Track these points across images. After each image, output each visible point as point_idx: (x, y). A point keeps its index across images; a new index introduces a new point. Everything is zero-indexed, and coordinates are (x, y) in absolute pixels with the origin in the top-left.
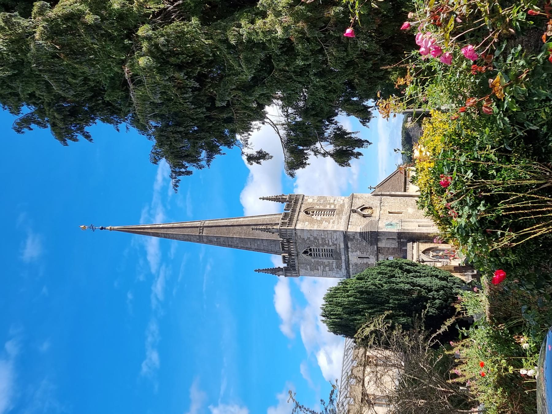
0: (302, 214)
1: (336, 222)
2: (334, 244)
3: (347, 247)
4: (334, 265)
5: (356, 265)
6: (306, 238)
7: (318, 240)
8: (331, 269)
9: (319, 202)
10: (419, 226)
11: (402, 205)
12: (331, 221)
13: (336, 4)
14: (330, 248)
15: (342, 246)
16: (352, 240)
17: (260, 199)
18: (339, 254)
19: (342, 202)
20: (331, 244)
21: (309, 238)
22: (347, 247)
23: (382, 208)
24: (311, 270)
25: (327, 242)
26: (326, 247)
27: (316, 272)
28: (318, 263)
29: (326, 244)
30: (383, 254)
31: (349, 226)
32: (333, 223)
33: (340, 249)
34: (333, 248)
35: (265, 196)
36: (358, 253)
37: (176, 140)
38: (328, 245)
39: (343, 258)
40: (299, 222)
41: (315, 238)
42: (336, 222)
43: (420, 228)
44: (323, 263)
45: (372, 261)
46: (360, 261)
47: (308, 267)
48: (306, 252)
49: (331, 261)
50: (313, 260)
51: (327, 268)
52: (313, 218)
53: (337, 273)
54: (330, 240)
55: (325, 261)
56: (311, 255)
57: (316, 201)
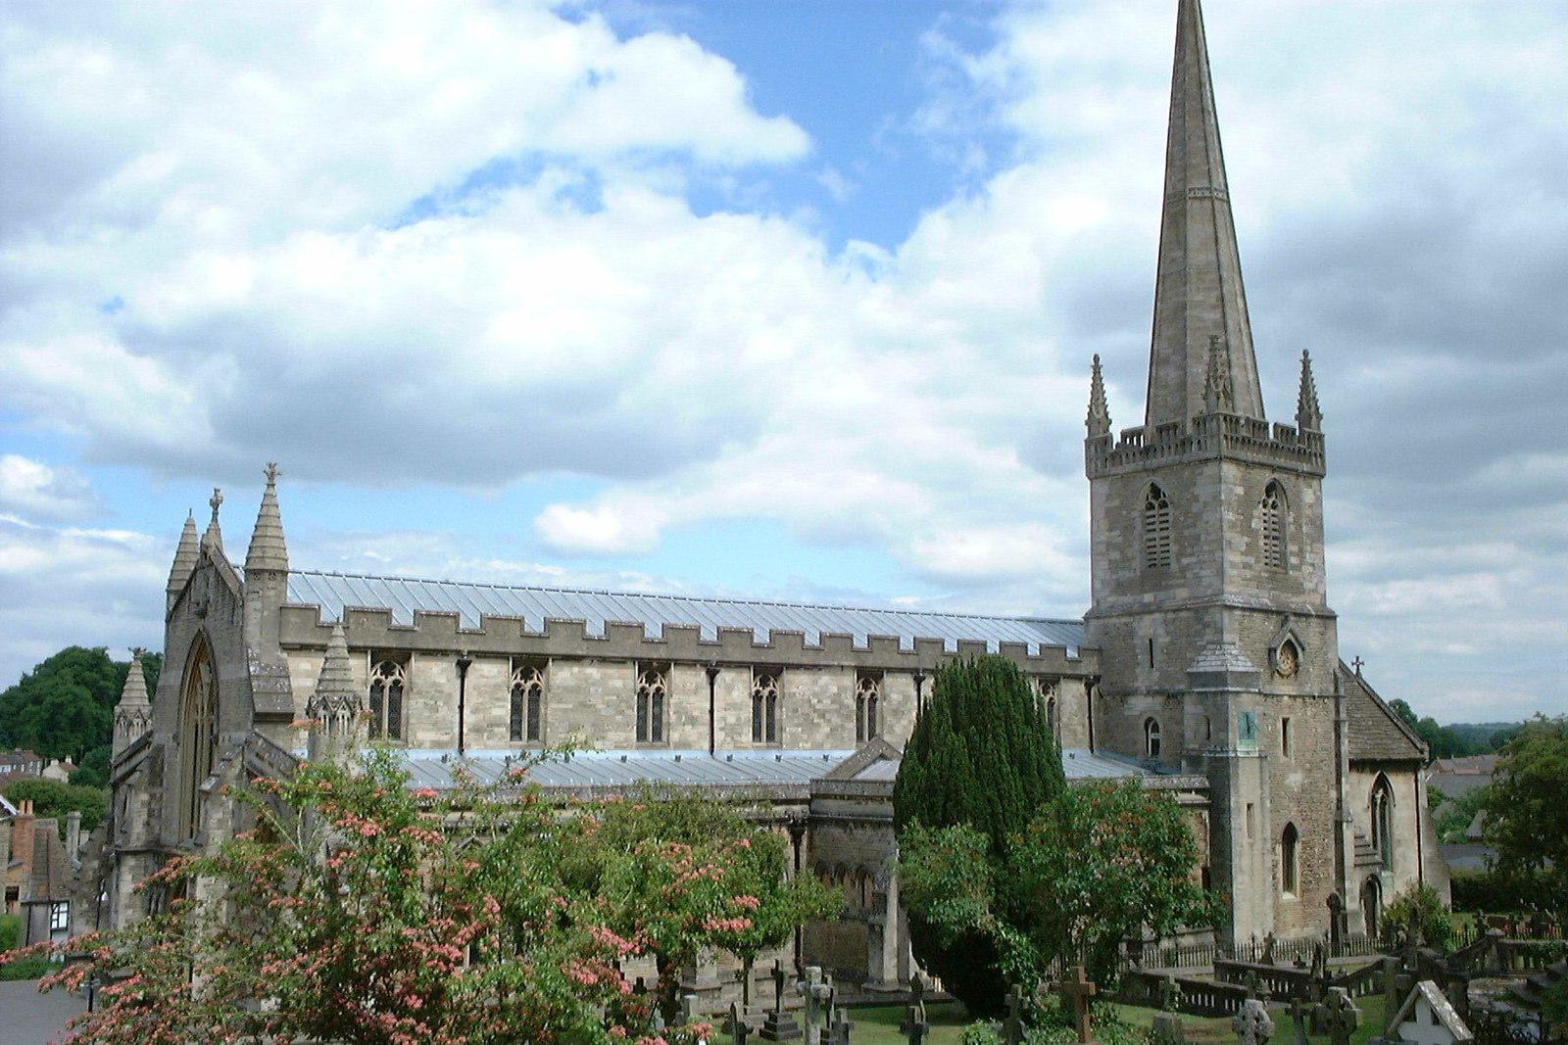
0: (1267, 477)
2: (1183, 570)
5: (1131, 633)
6: (1197, 491)
8: (1114, 566)
10: (1249, 806)
12: (1251, 560)
14: (1172, 561)
20: (1185, 561)
21: (1196, 499)
24: (1108, 511)
26: (1174, 548)
32: (1246, 566)
34: (1174, 567)
35: (1312, 367)
38: (1180, 555)
42: (1248, 574)
46: (1139, 642)
47: (1116, 503)
48: (1156, 491)
50: (1135, 514)
51: (1115, 555)
55: (1137, 546)
56: (1150, 507)
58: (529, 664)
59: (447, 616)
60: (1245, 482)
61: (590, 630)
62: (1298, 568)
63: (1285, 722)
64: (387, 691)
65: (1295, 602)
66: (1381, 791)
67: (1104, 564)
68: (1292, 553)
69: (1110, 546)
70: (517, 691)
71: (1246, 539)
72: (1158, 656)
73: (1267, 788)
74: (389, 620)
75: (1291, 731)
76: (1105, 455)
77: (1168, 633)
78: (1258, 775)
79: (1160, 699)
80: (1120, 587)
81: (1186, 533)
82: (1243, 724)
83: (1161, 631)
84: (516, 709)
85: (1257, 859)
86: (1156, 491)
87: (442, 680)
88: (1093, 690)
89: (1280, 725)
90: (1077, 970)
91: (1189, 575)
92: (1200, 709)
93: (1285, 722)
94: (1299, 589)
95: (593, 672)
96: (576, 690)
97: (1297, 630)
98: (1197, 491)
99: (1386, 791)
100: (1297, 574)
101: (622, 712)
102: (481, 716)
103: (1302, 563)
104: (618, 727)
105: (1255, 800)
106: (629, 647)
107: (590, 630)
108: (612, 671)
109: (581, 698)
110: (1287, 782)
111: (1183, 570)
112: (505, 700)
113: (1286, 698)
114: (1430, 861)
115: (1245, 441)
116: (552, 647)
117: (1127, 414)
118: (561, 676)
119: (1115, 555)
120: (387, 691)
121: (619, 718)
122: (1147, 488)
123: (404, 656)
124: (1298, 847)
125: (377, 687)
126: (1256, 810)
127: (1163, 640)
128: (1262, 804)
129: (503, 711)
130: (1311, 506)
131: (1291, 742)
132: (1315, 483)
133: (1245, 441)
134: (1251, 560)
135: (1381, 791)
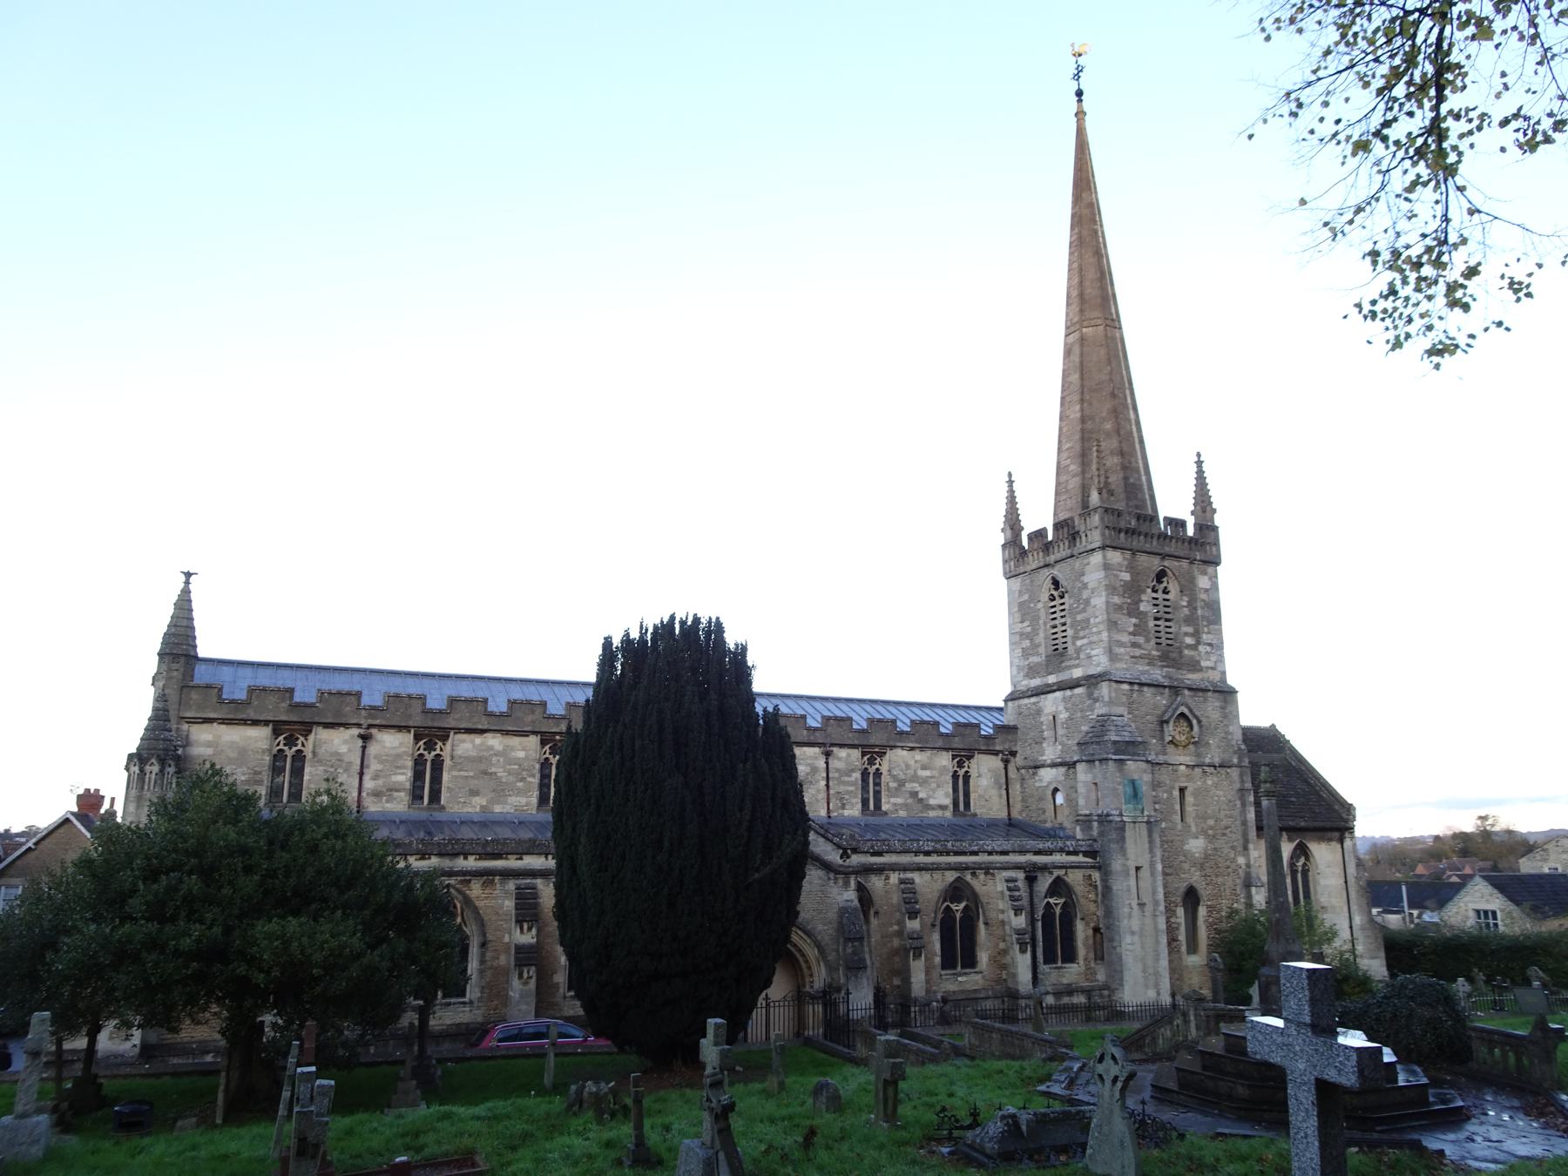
0: (1155, 563)
1: (1138, 652)
2: (1078, 650)
3: (1072, 685)
4: (1035, 659)
5: (1039, 712)
6: (1085, 579)
7: (1084, 610)
8: (1026, 654)
9: (1199, 604)
10: (1138, 869)
11: (1211, 822)
12: (1141, 640)
13: (950, 1130)
14: (1069, 645)
15: (1077, 673)
16: (1090, 695)
17: (1199, 455)
18: (1058, 669)
19: (1204, 664)
20: (1079, 643)
21: (1085, 586)
22: (1072, 685)
23: (1198, 770)
24: (1021, 605)
25: (1082, 634)
26: (1070, 632)
27: (1018, 617)
28: (1035, 619)
29: (1077, 631)
30: (1067, 775)
31: (1126, 687)
32: (1135, 645)
33: (1069, 668)
34: (1071, 650)
35: (1205, 467)
36: (1063, 716)
37: (1393, 292)
38: (1076, 638)
39: (1052, 679)
40: (1128, 554)
41: (1087, 602)
42: (1138, 652)
43: (1133, 872)
44: (1035, 632)
45: (1050, 753)
46: (1045, 719)
47: (1026, 597)
48: (1056, 583)
49: (1042, 650)
50: (1040, 605)
51: (1027, 643)
52: (1144, 592)
53: (1020, 669)
54: (1085, 641)
55: (1042, 635)
56: (1052, 598)
57: (1203, 596)
58: (431, 733)
59: (349, 694)
60: (1131, 568)
61: (492, 707)
62: (1194, 647)
63: (1182, 790)
64: (289, 760)
65: (1192, 678)
66: (1303, 860)
67: (1019, 652)
68: (1186, 634)
69: (1022, 635)
70: (419, 762)
71: (1134, 620)
72: (1061, 731)
73: (1158, 853)
74: (291, 698)
75: (1189, 799)
76: (1021, 552)
77: (1067, 709)
78: (1146, 839)
79: (1062, 770)
80: (1032, 671)
81: (1079, 617)
82: (1129, 790)
83: (1061, 708)
84: (418, 775)
85: (1148, 921)
86: (1056, 583)
87: (343, 749)
88: (1011, 767)
89: (1176, 793)
90: (537, 1015)
91: (1082, 656)
92: (1089, 777)
93: (1182, 790)
94: (1195, 666)
95: (495, 741)
96: (480, 759)
97: (1192, 705)
98: (1085, 579)
99: (1307, 858)
100: (1192, 653)
101: (523, 780)
102: (380, 782)
103: (1198, 643)
104: (519, 792)
105: (1144, 861)
106: (528, 721)
107: (492, 707)
108: (515, 741)
109: (483, 767)
110: (1186, 847)
111: (1078, 650)
112: (404, 767)
113: (1183, 768)
114: (1363, 929)
115: (1131, 532)
116: (450, 722)
117: (1039, 515)
118: (464, 746)
119: (1027, 643)
120: (289, 760)
121: (520, 784)
122: (1049, 582)
123: (307, 727)
124: (1202, 911)
125: (279, 756)
126: (1145, 873)
127: (1063, 716)
128: (1152, 865)
129: (404, 777)
130: (1207, 591)
131: (1189, 809)
132: (1210, 569)
133: (1131, 532)
134: (1141, 640)
135: (1303, 860)
